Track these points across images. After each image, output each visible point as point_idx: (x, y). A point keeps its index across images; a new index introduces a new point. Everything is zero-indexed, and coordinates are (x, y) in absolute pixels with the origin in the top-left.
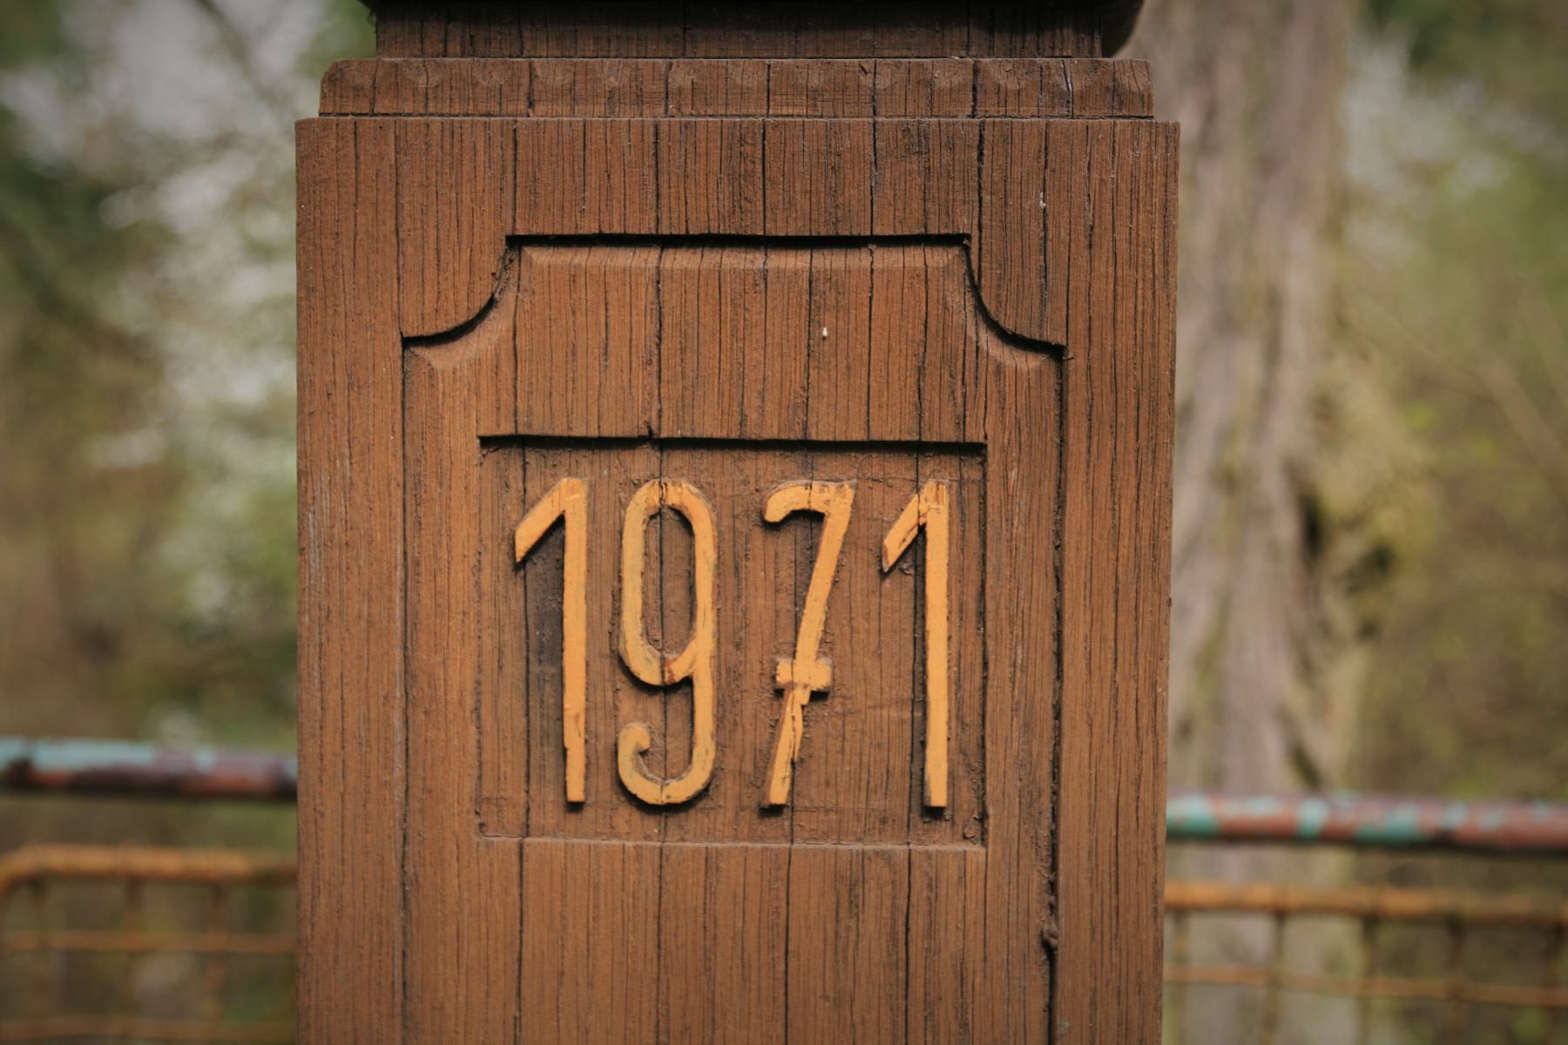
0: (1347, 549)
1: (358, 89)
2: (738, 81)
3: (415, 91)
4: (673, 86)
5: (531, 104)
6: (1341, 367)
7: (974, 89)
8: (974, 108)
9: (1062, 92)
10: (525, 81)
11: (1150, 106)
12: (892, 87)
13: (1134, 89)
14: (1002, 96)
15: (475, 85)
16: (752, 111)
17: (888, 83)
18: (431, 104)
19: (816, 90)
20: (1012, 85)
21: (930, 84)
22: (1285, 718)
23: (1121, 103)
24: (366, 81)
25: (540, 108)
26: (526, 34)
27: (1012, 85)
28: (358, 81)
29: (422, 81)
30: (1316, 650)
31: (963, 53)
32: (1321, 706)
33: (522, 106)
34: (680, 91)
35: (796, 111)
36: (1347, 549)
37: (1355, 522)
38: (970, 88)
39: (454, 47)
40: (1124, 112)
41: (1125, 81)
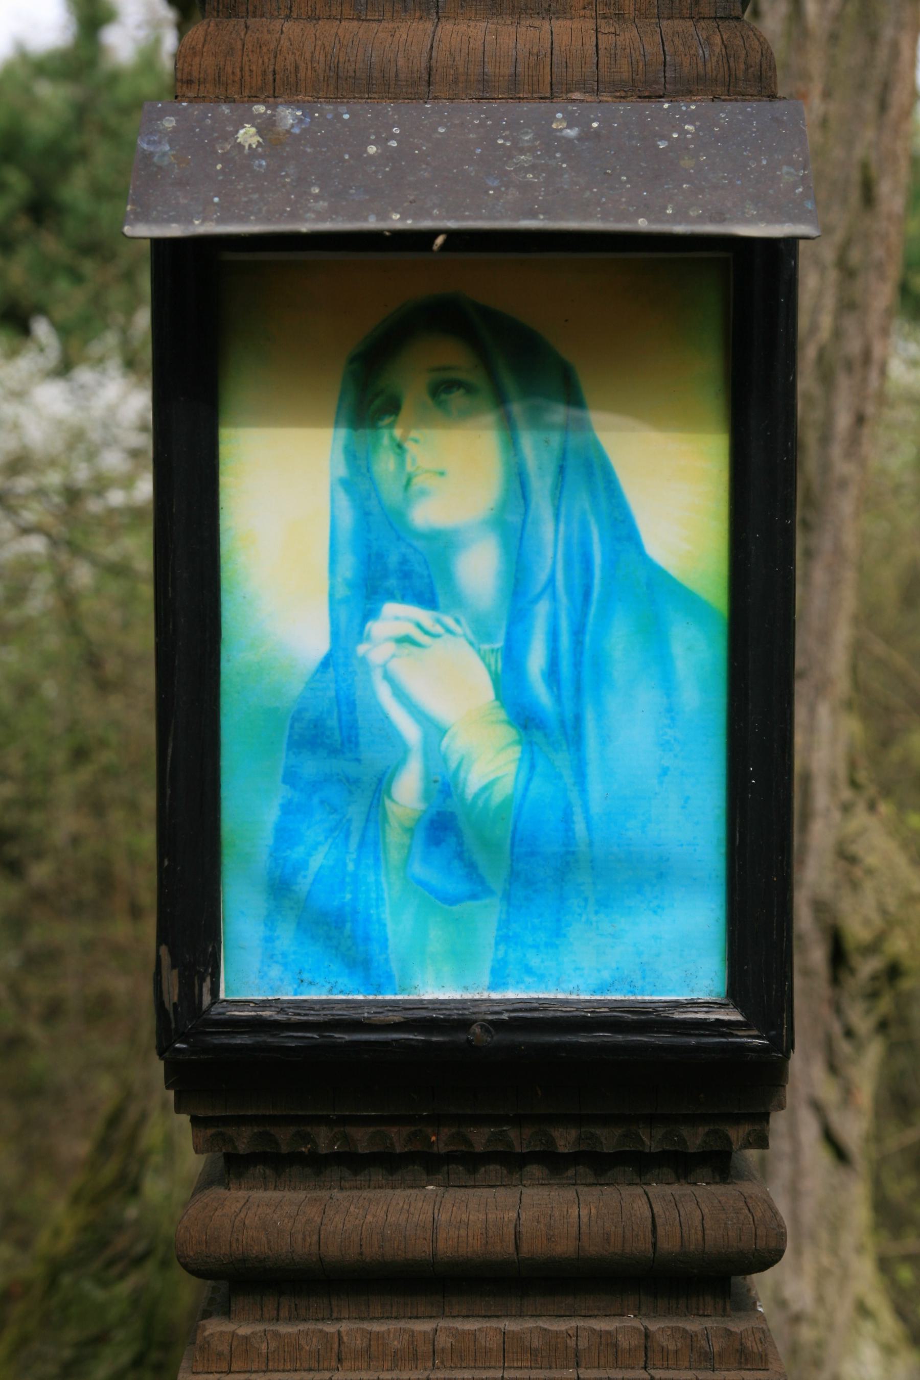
0: (867, 968)
1: (220, 1355)
2: (483, 1343)
3: (259, 1354)
4: (438, 1347)
5: (340, 1360)
6: (861, 818)
7: (646, 1347)
8: (646, 1362)
9: (706, 1352)
10: (336, 1346)
11: (766, 1362)
12: (589, 1348)
13: (755, 1350)
14: (665, 1354)
15: (301, 1349)
16: (493, 1364)
17: (586, 1345)
18: (270, 1364)
19: (536, 1350)
20: (672, 1347)
21: (615, 1345)
22: (817, 1107)
23: (746, 1360)
24: (225, 1348)
25: (347, 1364)
26: (334, 1303)
27: (672, 1347)
28: (220, 1348)
29: (264, 1346)
30: (845, 1047)
31: (636, 1313)
32: (848, 1093)
33: (334, 1364)
34: (443, 1350)
35: (524, 1364)
36: (867, 968)
37: (872, 948)
38: (643, 1349)
39: (284, 1313)
40: (749, 1366)
41: (749, 1344)
